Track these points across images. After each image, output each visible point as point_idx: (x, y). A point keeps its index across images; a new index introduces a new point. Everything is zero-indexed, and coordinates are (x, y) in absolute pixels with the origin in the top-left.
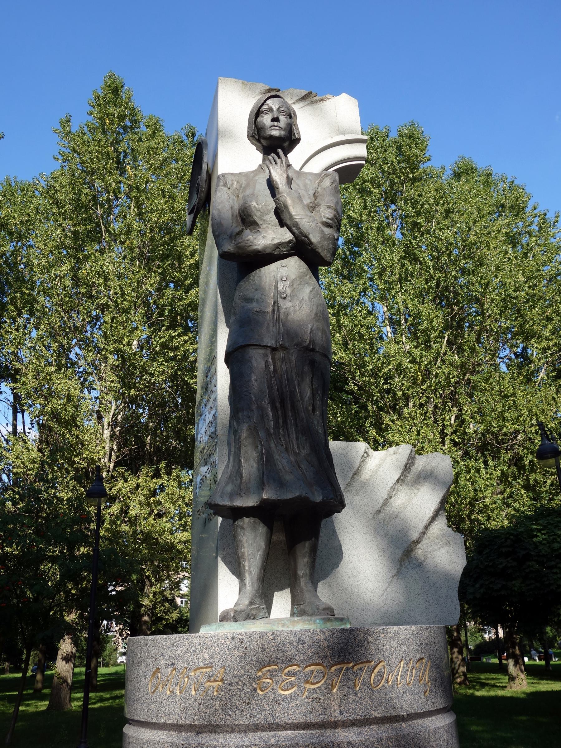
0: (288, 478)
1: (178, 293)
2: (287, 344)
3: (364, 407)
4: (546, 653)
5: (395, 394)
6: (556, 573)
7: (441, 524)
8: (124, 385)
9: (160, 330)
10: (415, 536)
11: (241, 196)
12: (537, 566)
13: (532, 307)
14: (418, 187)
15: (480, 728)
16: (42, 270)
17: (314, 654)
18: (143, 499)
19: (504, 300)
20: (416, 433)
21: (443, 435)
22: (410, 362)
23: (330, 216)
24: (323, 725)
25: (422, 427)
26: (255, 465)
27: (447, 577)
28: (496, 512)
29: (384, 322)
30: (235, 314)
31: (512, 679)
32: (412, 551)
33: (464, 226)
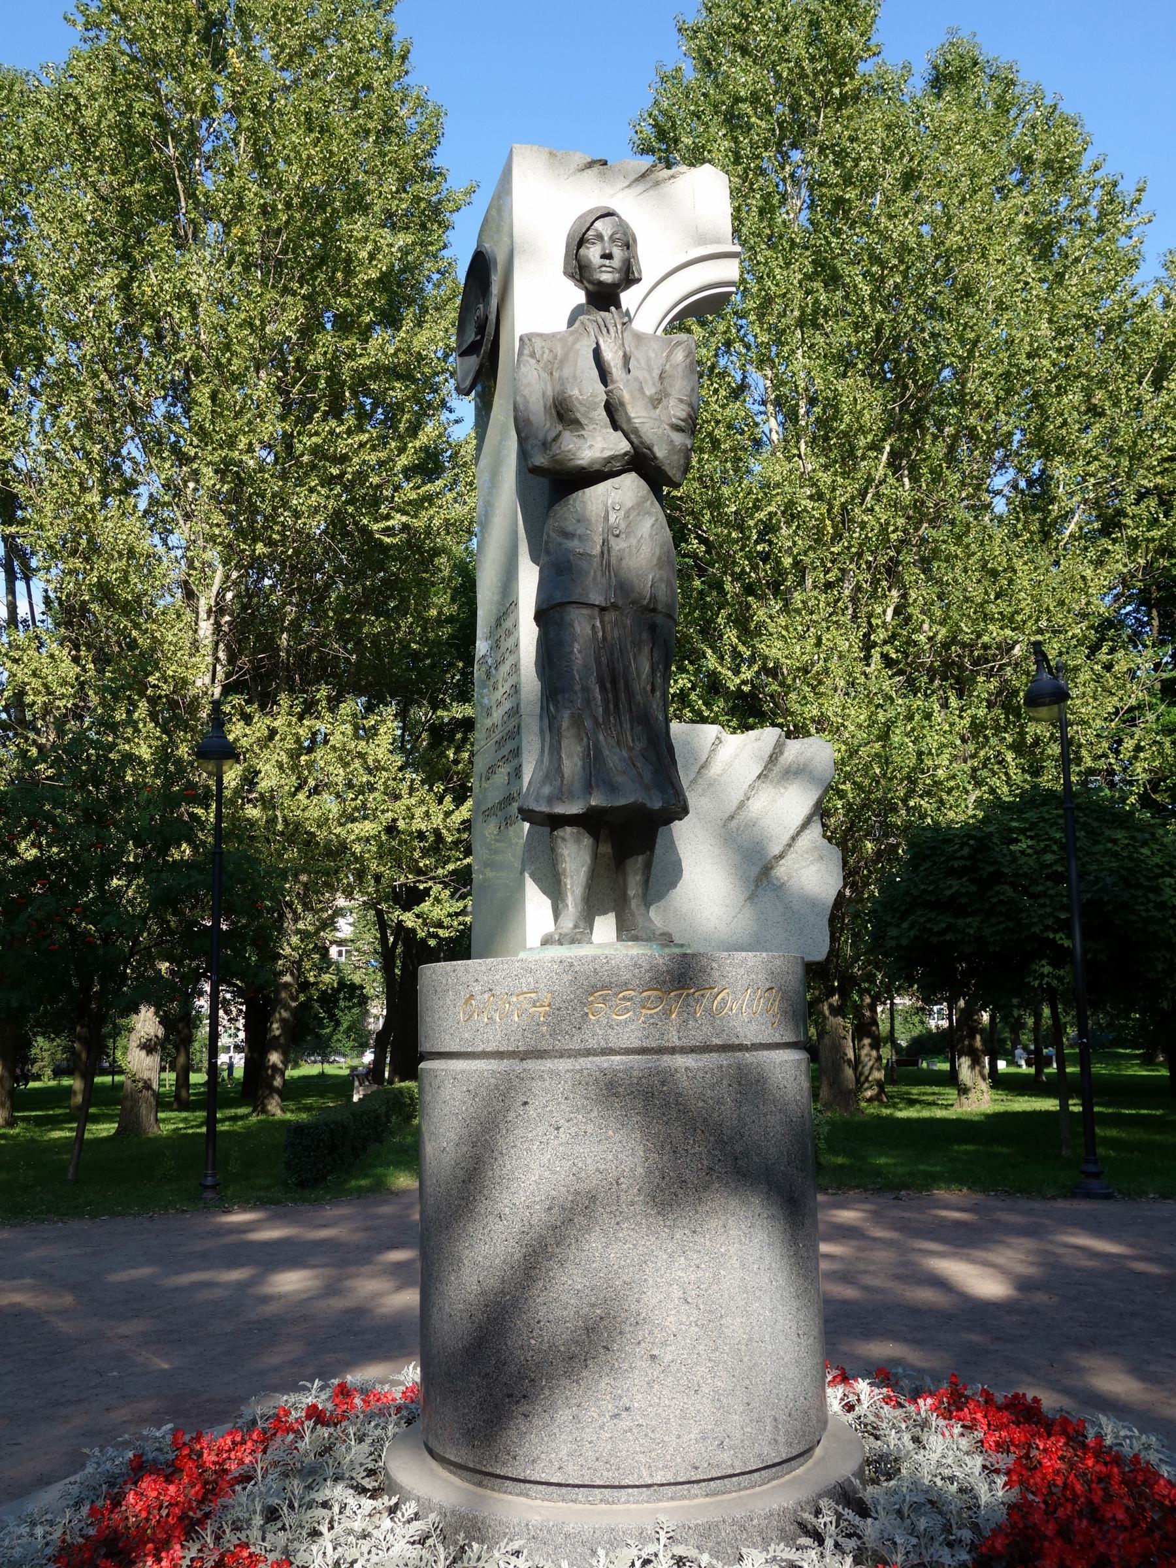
0: (620, 779)
1: (346, 343)
2: (620, 603)
3: (719, 586)
4: (1038, 1051)
5: (778, 562)
6: (1044, 905)
7: (815, 830)
8: (240, 533)
9: (310, 419)
10: (776, 850)
11: (556, 375)
12: (1010, 892)
13: (1061, 391)
14: (850, 118)
15: (891, 1161)
16: (57, 286)
17: (651, 979)
18: (284, 758)
19: (1007, 375)
20: (813, 641)
21: (868, 646)
22: (811, 497)
23: (683, 415)
24: (660, 1051)
25: (828, 628)
26: (580, 763)
27: (812, 903)
28: (956, 793)
29: (764, 403)
30: (548, 552)
31: (964, 1091)
32: (772, 868)
33: (938, 210)
